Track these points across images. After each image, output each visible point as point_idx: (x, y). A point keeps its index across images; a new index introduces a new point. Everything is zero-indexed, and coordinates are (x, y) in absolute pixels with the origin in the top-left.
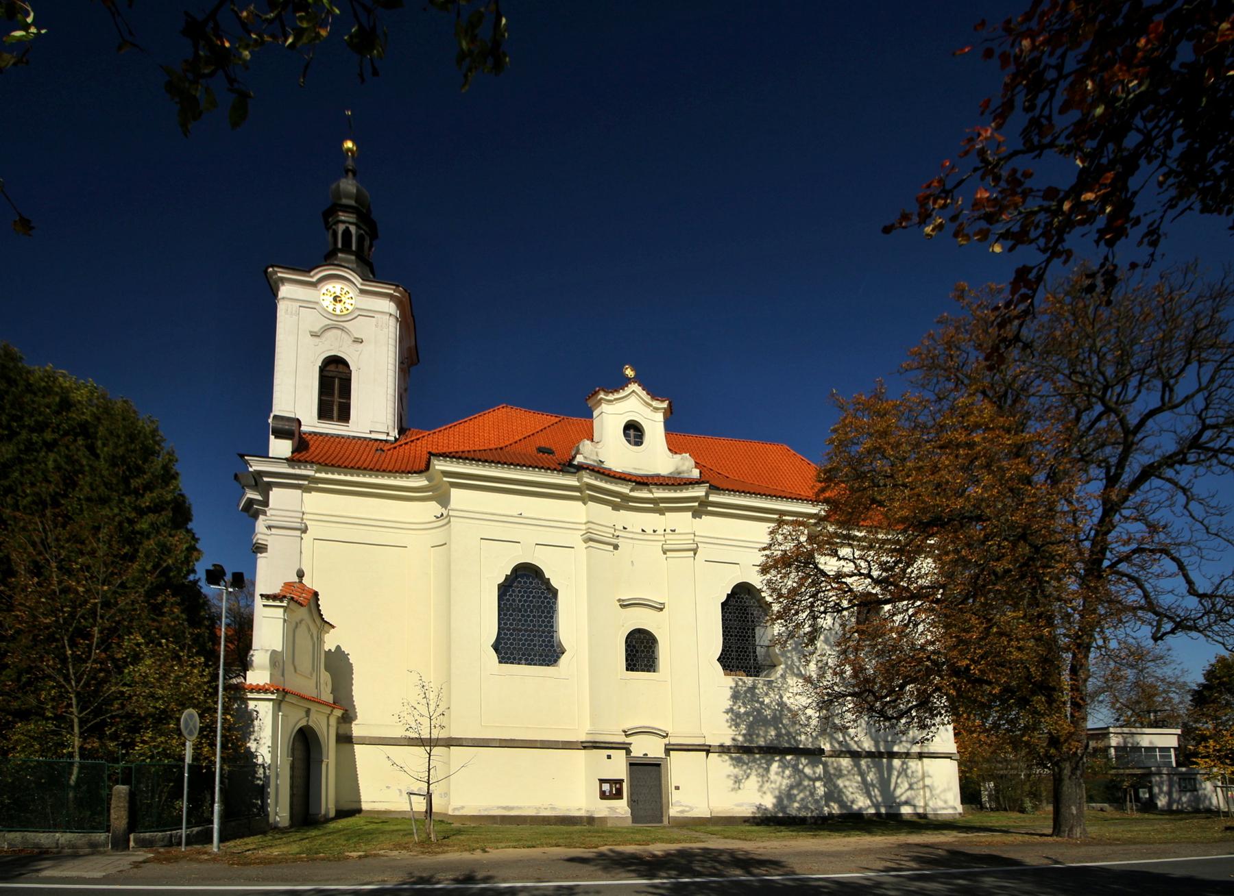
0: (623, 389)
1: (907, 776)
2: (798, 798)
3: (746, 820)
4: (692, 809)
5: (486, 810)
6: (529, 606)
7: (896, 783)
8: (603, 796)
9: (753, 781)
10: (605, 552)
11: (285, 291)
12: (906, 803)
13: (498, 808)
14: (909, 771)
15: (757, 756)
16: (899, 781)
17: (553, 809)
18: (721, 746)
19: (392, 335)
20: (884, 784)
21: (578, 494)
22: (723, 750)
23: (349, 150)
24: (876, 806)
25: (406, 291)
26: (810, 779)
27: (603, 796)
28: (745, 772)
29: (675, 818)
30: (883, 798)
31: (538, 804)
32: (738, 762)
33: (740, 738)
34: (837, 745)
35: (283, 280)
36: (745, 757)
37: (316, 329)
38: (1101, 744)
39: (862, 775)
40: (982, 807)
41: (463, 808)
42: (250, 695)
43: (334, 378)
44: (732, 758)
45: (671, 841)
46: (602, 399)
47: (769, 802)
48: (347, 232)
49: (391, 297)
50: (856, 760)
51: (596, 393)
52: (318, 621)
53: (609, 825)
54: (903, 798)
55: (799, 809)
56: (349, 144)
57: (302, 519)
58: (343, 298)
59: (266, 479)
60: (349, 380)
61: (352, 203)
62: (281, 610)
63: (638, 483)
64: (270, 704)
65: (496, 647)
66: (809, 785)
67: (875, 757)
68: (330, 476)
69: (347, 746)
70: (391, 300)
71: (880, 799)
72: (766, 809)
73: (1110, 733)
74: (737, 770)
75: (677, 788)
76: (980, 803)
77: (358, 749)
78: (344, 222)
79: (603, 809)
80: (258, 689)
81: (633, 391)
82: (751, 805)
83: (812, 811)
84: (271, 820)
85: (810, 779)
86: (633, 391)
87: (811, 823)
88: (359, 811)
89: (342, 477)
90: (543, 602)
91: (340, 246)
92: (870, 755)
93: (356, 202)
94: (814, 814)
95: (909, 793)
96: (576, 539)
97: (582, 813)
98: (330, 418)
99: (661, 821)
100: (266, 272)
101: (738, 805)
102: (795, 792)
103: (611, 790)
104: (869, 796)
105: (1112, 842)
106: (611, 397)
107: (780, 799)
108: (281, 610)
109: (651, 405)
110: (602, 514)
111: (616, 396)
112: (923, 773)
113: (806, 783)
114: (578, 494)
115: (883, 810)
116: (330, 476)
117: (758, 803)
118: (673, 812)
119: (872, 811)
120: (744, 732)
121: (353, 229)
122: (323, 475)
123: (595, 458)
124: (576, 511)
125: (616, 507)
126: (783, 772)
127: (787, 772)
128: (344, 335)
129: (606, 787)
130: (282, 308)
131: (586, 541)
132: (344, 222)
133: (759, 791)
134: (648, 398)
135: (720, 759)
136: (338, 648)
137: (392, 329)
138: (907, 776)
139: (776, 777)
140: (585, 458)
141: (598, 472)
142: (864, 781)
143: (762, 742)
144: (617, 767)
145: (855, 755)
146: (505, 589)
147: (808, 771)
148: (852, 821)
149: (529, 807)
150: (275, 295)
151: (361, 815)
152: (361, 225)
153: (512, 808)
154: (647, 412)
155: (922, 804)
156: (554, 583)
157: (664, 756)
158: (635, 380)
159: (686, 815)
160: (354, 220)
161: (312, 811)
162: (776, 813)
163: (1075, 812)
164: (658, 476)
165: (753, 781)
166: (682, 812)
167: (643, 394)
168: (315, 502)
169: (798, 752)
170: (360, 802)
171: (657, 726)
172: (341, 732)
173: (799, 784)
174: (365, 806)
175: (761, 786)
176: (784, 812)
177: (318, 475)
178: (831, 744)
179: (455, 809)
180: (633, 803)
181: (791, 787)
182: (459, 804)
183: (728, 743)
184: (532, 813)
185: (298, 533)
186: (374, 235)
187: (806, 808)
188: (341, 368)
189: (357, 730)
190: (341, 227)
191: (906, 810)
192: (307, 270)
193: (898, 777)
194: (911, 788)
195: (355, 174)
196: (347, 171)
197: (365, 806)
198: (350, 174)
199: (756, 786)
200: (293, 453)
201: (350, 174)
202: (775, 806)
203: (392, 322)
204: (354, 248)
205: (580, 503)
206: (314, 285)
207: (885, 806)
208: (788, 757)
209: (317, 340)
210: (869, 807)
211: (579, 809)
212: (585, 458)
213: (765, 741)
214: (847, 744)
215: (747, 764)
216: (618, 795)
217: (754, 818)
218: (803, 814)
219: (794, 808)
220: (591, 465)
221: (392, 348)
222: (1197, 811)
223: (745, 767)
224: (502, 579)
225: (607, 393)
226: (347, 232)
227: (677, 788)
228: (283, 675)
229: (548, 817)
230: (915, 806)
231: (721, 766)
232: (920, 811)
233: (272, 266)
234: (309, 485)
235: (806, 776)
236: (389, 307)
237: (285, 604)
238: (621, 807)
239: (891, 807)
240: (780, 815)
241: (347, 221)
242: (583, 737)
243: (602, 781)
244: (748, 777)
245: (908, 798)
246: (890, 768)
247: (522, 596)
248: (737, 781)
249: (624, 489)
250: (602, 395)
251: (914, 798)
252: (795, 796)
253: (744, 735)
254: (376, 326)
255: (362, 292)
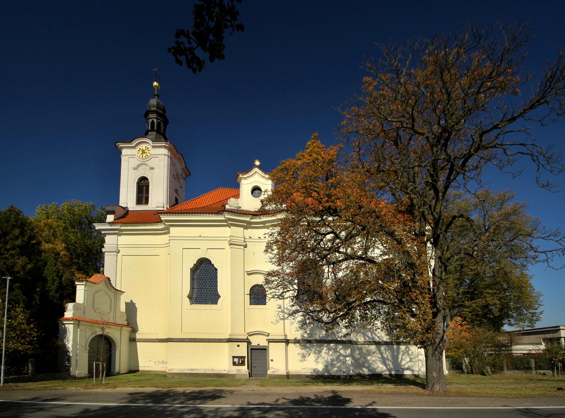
0: (250, 171)
1: (408, 354)
2: (336, 366)
3: (307, 376)
4: (278, 370)
5: (182, 370)
6: (207, 277)
7: (402, 358)
8: (234, 364)
9: (312, 357)
10: (240, 250)
11: (124, 152)
12: (408, 369)
13: (188, 369)
14: (410, 352)
15: (315, 344)
16: (404, 357)
17: (213, 370)
18: (295, 339)
19: (166, 163)
20: (395, 359)
21: (226, 223)
22: (296, 341)
23: (156, 86)
24: (390, 370)
25: (171, 143)
26: (343, 356)
27: (234, 364)
28: (308, 352)
29: (270, 375)
30: (394, 366)
31: (206, 368)
32: (305, 347)
33: (306, 335)
34: (367, 338)
35: (122, 148)
36: (308, 345)
37: (135, 166)
38: (555, 335)
39: (381, 353)
40: (463, 372)
41: (172, 369)
42: (65, 322)
43: (143, 186)
44: (301, 345)
45: (215, 386)
46: (241, 178)
47: (320, 367)
48: (153, 123)
49: (165, 147)
50: (378, 346)
51: (238, 175)
52: (113, 290)
53: (237, 378)
54: (406, 366)
55: (337, 371)
56: (155, 84)
57: (117, 247)
58: (146, 151)
59: (102, 232)
60: (148, 186)
61: (155, 109)
62: (83, 286)
63: (253, 215)
64: (72, 325)
65: (190, 297)
66: (343, 359)
67: (389, 344)
68: (126, 228)
69: (133, 343)
70: (165, 148)
71: (391, 366)
72: (318, 371)
73: (560, 329)
74: (303, 351)
75: (272, 360)
76: (462, 369)
77: (138, 344)
78: (151, 118)
79: (234, 370)
80: (68, 319)
81: (256, 172)
82: (311, 369)
83: (344, 372)
84: (72, 374)
85: (343, 356)
86: (256, 172)
87: (343, 379)
88: (138, 371)
89: (131, 228)
90: (213, 275)
91: (150, 129)
92: (386, 343)
93: (157, 108)
94: (345, 374)
95: (409, 364)
96: (226, 244)
97: (226, 372)
98: (142, 204)
99: (266, 377)
100: (116, 145)
101: (303, 369)
102: (335, 363)
103: (238, 361)
104: (386, 365)
105: (487, 396)
106: (245, 176)
107: (326, 367)
108: (83, 286)
109: (265, 177)
110: (238, 232)
111: (248, 175)
112: (418, 353)
113: (341, 358)
114: (226, 223)
115: (393, 373)
116: (126, 228)
117: (314, 368)
118: (269, 372)
119: (387, 373)
120: (308, 332)
121: (155, 120)
122: (123, 228)
123: (236, 206)
124: (226, 232)
125: (246, 228)
126: (329, 352)
127: (331, 352)
128: (147, 167)
129: (236, 360)
130: (123, 158)
131: (231, 244)
132: (151, 118)
133: (315, 361)
134: (263, 174)
135: (295, 345)
136: (131, 301)
137: (166, 161)
138: (408, 354)
139: (325, 355)
140: (230, 206)
141: (232, 212)
142: (383, 357)
143: (318, 338)
144: (242, 351)
145: (378, 344)
146: (194, 271)
147: (342, 352)
148: (376, 378)
149: (202, 369)
150: (121, 153)
151: (139, 372)
152: (159, 118)
153: (194, 370)
154: (263, 181)
155: (417, 369)
156: (215, 266)
157: (267, 345)
158: (259, 167)
159: (275, 373)
160: (155, 116)
161: (112, 370)
162: (324, 373)
163: (435, 376)
164: (249, 211)
165: (312, 357)
166: (274, 372)
167: (260, 172)
168: (123, 240)
169: (337, 342)
170: (138, 367)
171: (258, 330)
172: (132, 337)
173: (338, 358)
174: (141, 369)
175: (316, 359)
176: (328, 373)
177: (122, 228)
178: (364, 337)
179: (169, 370)
180: (250, 367)
181: (333, 360)
182: (171, 368)
183: (299, 337)
184: (203, 372)
185: (243, 247)
186: (166, 122)
187: (341, 371)
188: (146, 181)
189: (138, 336)
190: (150, 120)
191: (407, 373)
192: (131, 141)
193: (403, 355)
194: (411, 360)
195: (158, 96)
196: (155, 95)
197: (141, 369)
198: (156, 96)
199: (314, 359)
200: (114, 220)
201: (156, 96)
202: (323, 369)
203: (166, 158)
204: (155, 128)
205: (228, 228)
206: (134, 147)
207: (395, 370)
208: (332, 345)
209: (135, 171)
210: (385, 371)
211: (225, 370)
212: (230, 206)
213: (319, 337)
214: (373, 338)
215: (309, 348)
216: (243, 364)
217: (312, 375)
218: (339, 374)
219: (334, 371)
220: (233, 209)
221: (166, 170)
222: (427, 379)
223: (308, 350)
224: (192, 266)
225: (243, 174)
226: (153, 123)
227: (272, 360)
228: (84, 313)
229: (210, 374)
230: (413, 371)
231: (295, 349)
232: (416, 373)
233: (117, 142)
234: (120, 233)
235: (341, 354)
236: (165, 151)
237: (84, 283)
238: (244, 369)
239: (398, 371)
240: (326, 374)
241: (153, 117)
242: (228, 337)
243: (234, 357)
244: (309, 354)
245: (409, 366)
246: (398, 349)
247: (204, 273)
248: (304, 356)
249: (247, 219)
250: (241, 176)
251: (413, 366)
252: (335, 365)
253: (308, 334)
254: (159, 161)
255: (153, 147)
